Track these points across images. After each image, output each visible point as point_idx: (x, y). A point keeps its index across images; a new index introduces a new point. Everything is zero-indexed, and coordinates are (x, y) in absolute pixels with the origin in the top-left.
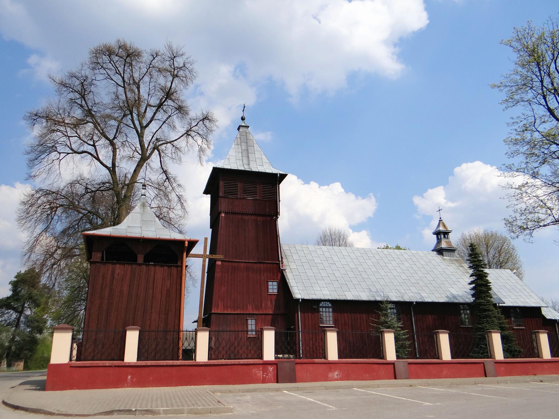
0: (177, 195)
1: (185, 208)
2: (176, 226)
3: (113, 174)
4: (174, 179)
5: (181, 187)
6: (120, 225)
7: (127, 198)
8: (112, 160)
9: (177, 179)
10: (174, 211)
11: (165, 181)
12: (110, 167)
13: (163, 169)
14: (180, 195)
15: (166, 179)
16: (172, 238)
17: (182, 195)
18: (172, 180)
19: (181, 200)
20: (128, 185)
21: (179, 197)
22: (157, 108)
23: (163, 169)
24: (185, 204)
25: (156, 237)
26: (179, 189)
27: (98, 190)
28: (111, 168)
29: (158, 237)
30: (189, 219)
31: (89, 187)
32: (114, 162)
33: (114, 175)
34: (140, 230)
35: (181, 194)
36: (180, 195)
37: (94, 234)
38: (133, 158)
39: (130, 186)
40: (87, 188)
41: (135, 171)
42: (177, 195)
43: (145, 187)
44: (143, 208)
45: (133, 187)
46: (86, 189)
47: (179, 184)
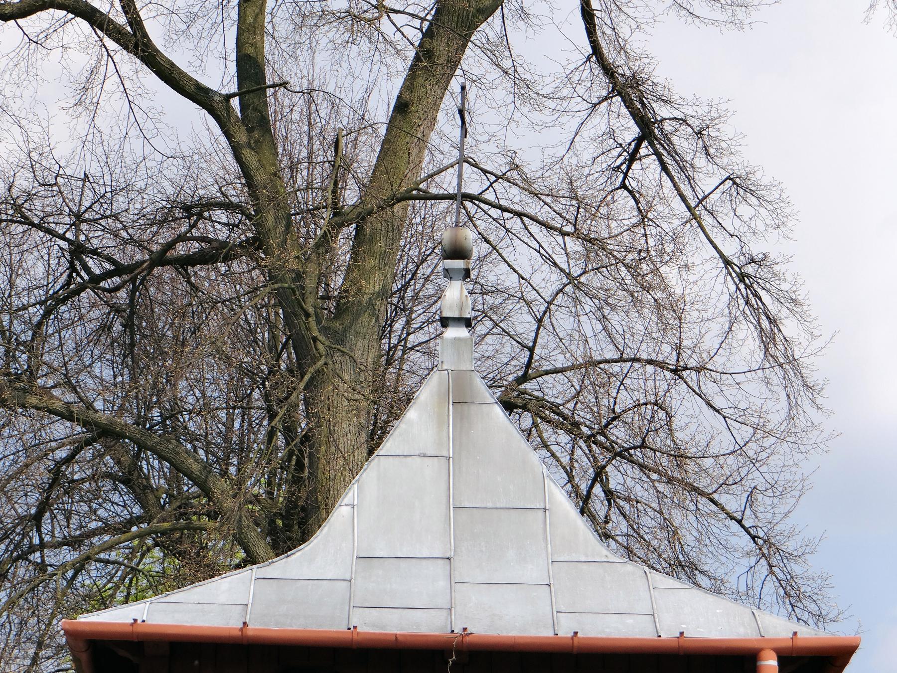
0: (727, 263)
1: (793, 361)
2: (732, 502)
3: (249, 146)
4: (699, 134)
5: (753, 200)
6: (306, 549)
7: (358, 315)
8: (235, 28)
9: (725, 131)
10: (709, 388)
11: (633, 157)
12: (229, 97)
13: (608, 71)
14: (753, 260)
15: (639, 141)
16: (664, 636)
17: (766, 256)
18: (683, 142)
19: (762, 293)
20: (361, 217)
21: (742, 277)
22: (201, 252)
23: (608, 71)
24: (790, 327)
25: (550, 634)
26: (744, 210)
27: (160, 259)
28: (235, 102)
29: (565, 632)
30: (830, 438)
31: (98, 239)
32: (250, 50)
33: (256, 147)
34: (443, 584)
35: (756, 249)
36: (753, 260)
37: (139, 629)
38: (385, 25)
39: (374, 224)
40: (78, 251)
41: (402, 107)
42: (727, 263)
43: (459, 264)
44: (461, 420)
45: (394, 231)
46: (72, 253)
47: (739, 170)
